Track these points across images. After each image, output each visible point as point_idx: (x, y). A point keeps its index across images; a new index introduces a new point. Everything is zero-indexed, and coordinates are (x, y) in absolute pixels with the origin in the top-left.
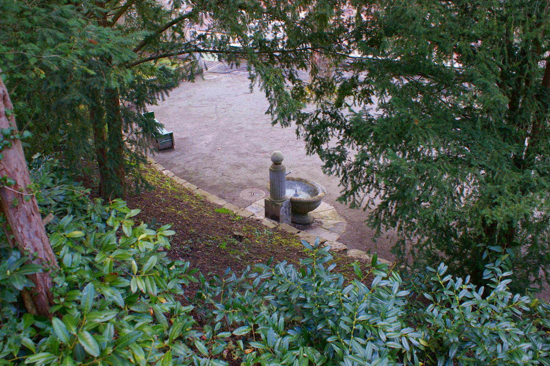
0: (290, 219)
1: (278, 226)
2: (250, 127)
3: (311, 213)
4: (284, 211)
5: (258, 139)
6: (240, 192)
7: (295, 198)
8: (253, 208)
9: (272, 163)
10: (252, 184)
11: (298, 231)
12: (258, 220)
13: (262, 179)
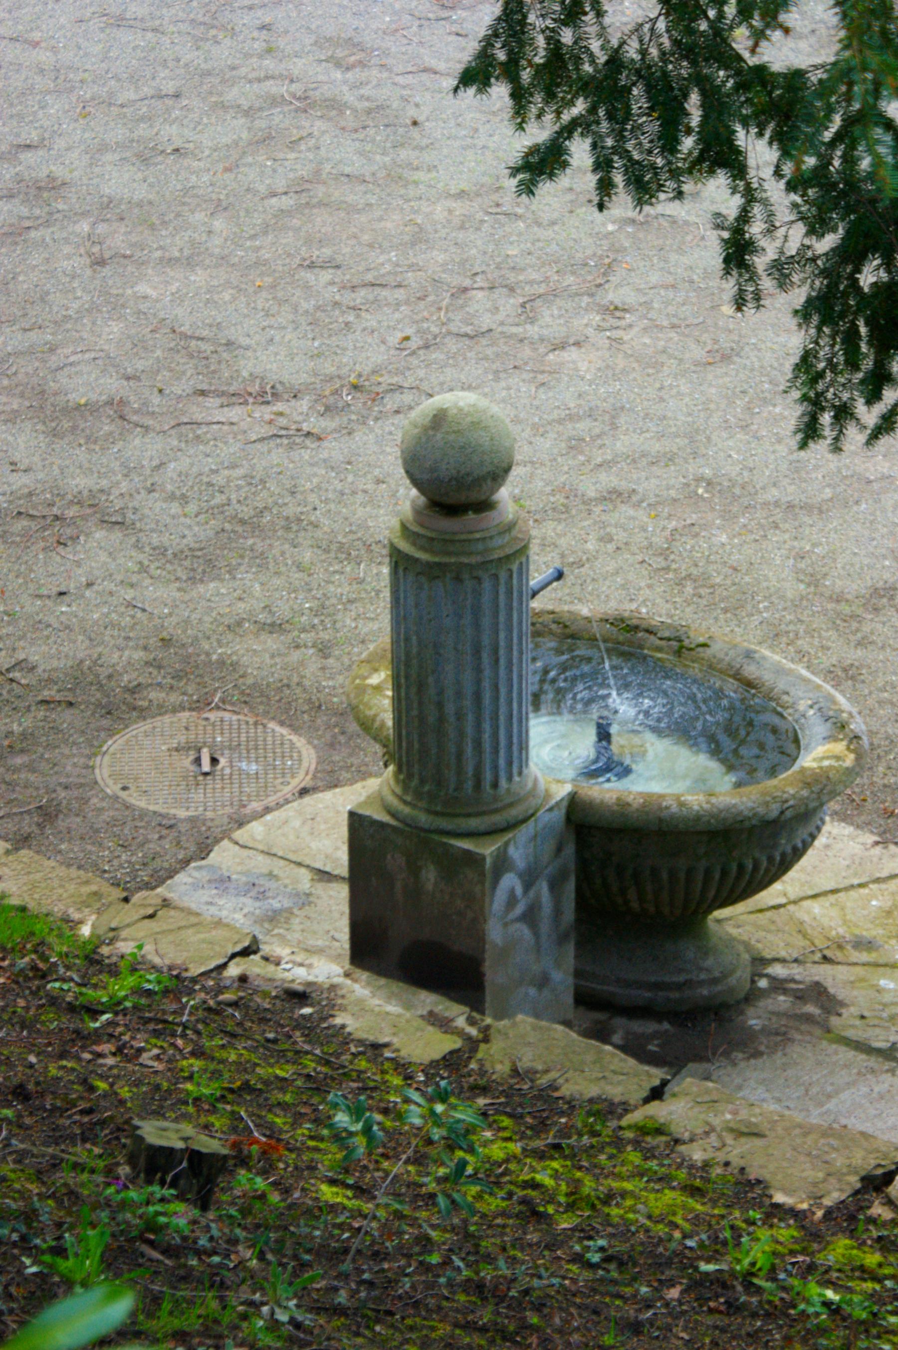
0: (562, 978)
1: (473, 1045)
2: (120, 181)
3: (737, 923)
4: (516, 911)
5: (199, 277)
6: (95, 750)
7: (606, 791)
8: (222, 882)
9: (408, 497)
10: (187, 675)
11: (656, 1075)
12: (299, 997)
13: (275, 628)
